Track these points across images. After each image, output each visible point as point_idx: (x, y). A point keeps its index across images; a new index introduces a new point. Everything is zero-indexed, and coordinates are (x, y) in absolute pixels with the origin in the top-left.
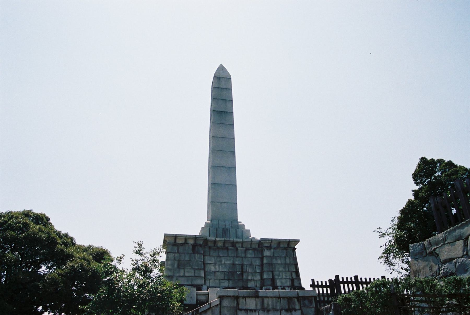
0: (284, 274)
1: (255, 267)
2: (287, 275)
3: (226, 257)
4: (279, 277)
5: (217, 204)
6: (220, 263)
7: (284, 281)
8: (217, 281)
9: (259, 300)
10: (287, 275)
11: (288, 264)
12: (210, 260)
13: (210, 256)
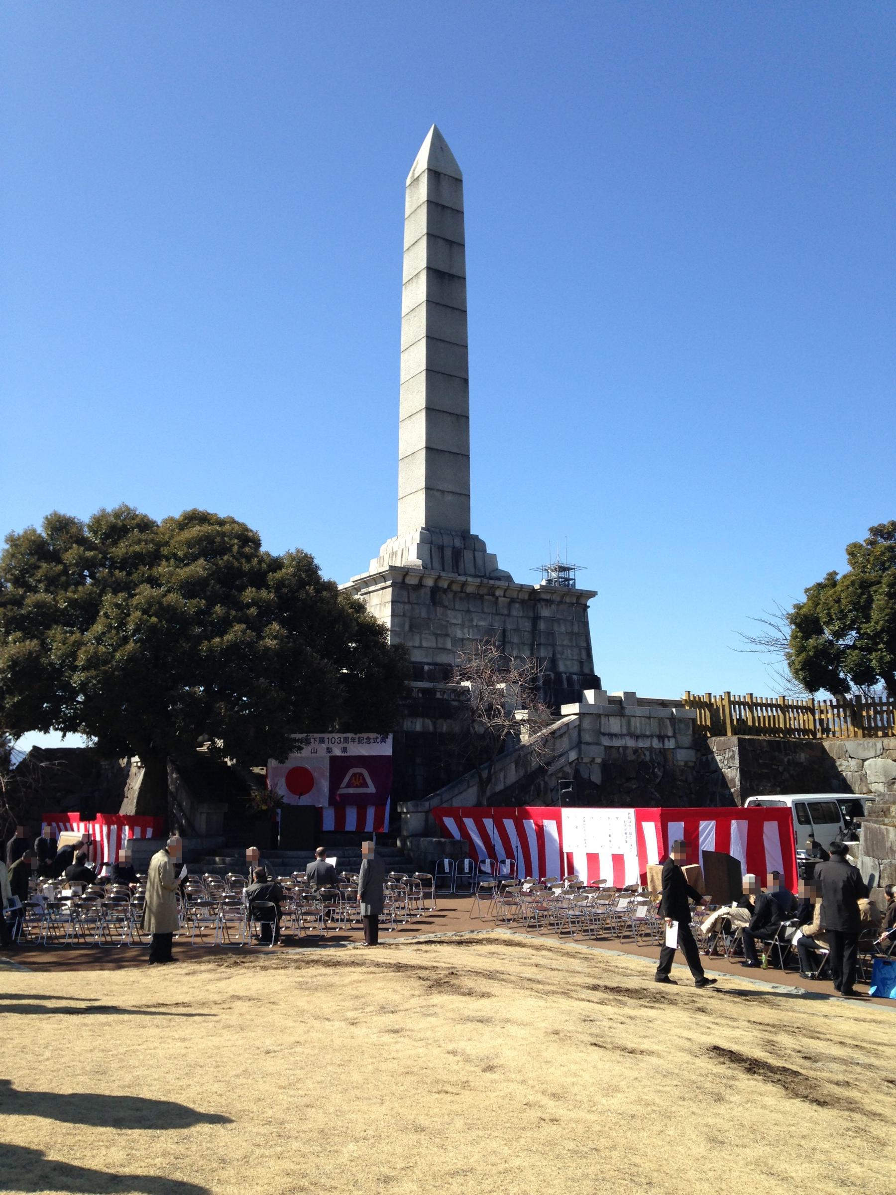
0: (569, 651)
7: (568, 663)
9: (624, 721)
11: (576, 634)
13: (454, 609)
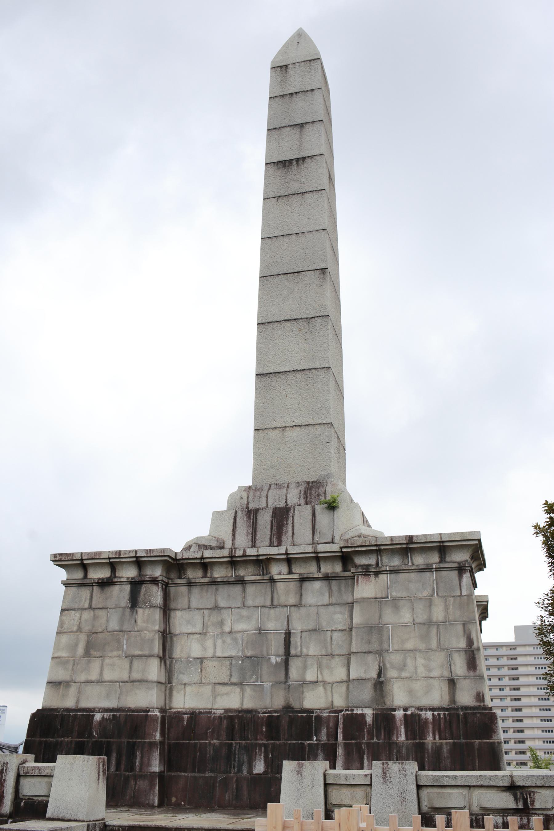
0: (420, 661)
1: (329, 639)
2: (433, 664)
4: (404, 674)
5: (271, 433)
6: (219, 631)
7: (418, 686)
8: (207, 690)
10: (433, 664)
11: (438, 624)
12: (189, 622)
13: (189, 609)
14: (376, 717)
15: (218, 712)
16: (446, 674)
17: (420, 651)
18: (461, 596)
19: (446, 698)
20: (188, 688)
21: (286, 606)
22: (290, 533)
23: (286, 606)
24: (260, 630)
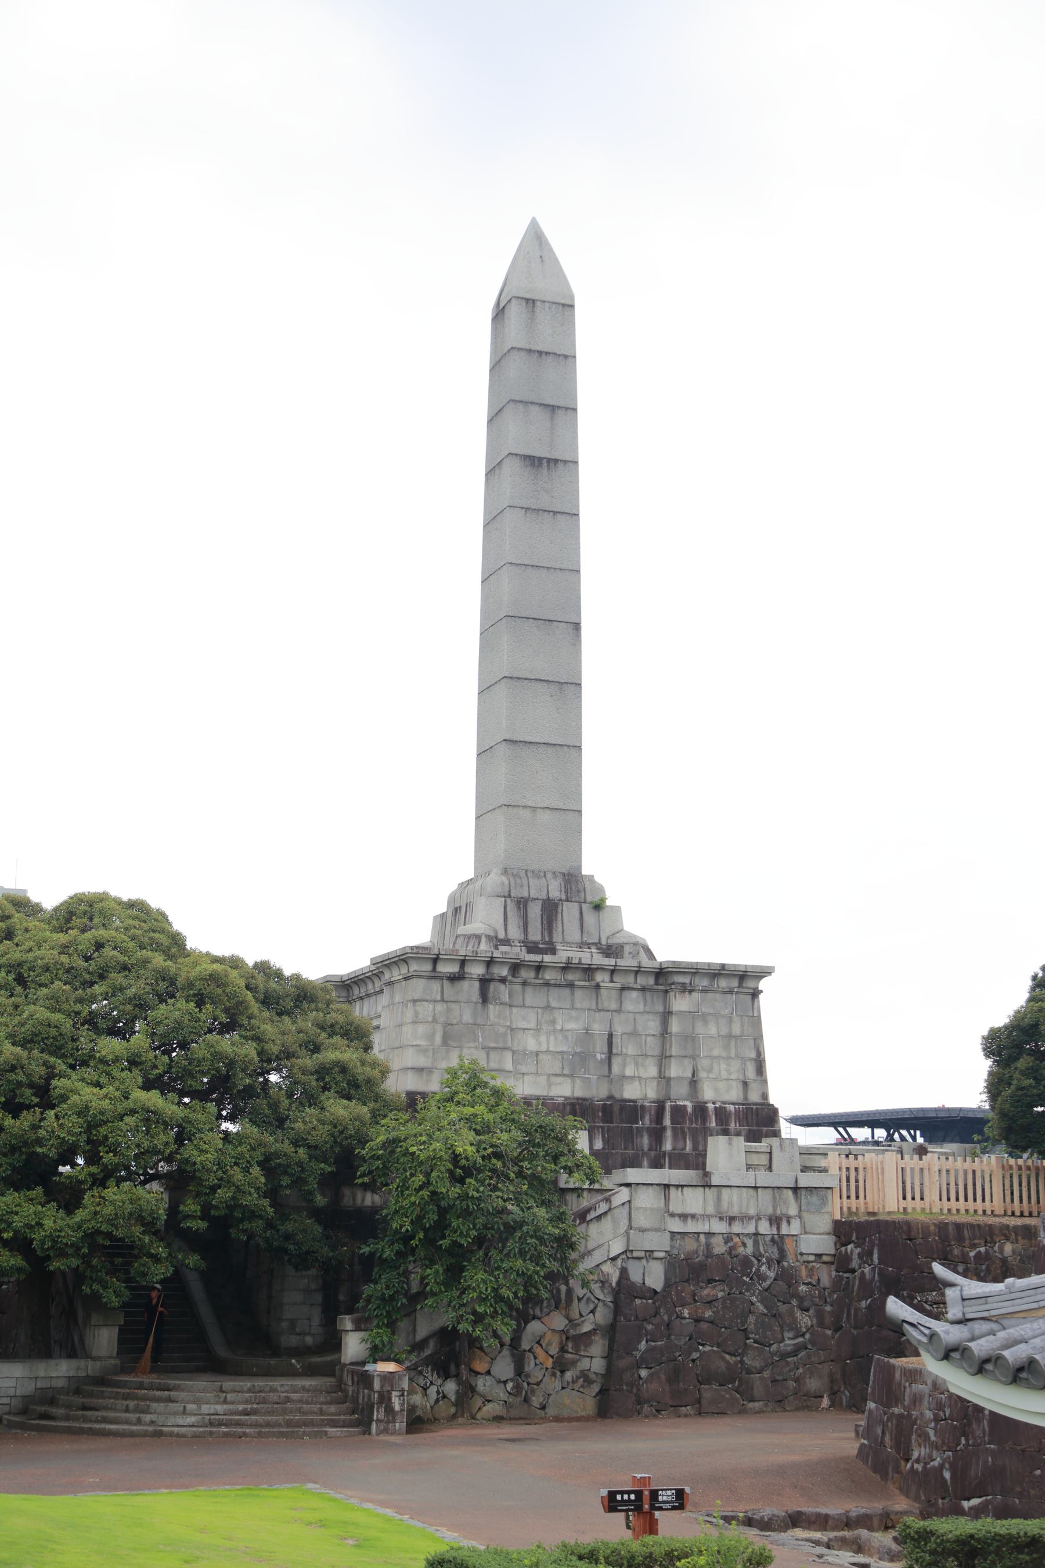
0: (723, 1066)
3: (567, 1011)
4: (711, 1076)
5: (521, 811)
6: (551, 1028)
7: (722, 1085)
8: (543, 1080)
11: (736, 1037)
13: (524, 1006)
14: (694, 1108)
15: (559, 1099)
16: (741, 1077)
17: (723, 1058)
18: (753, 1016)
19: (741, 1095)
20: (526, 1078)
21: (609, 1011)
22: (560, 929)
23: (609, 1011)
24: (587, 1030)
